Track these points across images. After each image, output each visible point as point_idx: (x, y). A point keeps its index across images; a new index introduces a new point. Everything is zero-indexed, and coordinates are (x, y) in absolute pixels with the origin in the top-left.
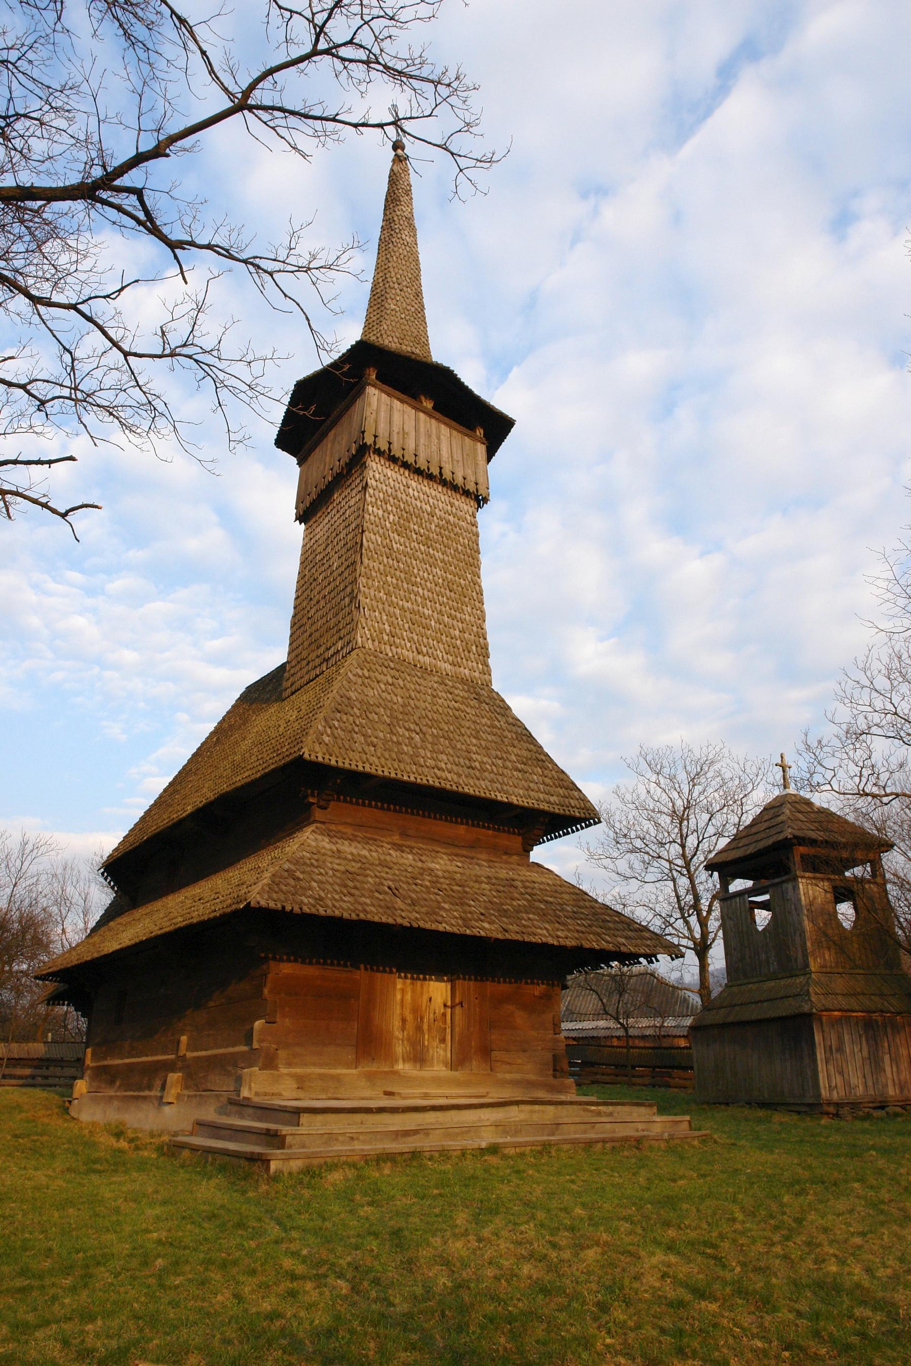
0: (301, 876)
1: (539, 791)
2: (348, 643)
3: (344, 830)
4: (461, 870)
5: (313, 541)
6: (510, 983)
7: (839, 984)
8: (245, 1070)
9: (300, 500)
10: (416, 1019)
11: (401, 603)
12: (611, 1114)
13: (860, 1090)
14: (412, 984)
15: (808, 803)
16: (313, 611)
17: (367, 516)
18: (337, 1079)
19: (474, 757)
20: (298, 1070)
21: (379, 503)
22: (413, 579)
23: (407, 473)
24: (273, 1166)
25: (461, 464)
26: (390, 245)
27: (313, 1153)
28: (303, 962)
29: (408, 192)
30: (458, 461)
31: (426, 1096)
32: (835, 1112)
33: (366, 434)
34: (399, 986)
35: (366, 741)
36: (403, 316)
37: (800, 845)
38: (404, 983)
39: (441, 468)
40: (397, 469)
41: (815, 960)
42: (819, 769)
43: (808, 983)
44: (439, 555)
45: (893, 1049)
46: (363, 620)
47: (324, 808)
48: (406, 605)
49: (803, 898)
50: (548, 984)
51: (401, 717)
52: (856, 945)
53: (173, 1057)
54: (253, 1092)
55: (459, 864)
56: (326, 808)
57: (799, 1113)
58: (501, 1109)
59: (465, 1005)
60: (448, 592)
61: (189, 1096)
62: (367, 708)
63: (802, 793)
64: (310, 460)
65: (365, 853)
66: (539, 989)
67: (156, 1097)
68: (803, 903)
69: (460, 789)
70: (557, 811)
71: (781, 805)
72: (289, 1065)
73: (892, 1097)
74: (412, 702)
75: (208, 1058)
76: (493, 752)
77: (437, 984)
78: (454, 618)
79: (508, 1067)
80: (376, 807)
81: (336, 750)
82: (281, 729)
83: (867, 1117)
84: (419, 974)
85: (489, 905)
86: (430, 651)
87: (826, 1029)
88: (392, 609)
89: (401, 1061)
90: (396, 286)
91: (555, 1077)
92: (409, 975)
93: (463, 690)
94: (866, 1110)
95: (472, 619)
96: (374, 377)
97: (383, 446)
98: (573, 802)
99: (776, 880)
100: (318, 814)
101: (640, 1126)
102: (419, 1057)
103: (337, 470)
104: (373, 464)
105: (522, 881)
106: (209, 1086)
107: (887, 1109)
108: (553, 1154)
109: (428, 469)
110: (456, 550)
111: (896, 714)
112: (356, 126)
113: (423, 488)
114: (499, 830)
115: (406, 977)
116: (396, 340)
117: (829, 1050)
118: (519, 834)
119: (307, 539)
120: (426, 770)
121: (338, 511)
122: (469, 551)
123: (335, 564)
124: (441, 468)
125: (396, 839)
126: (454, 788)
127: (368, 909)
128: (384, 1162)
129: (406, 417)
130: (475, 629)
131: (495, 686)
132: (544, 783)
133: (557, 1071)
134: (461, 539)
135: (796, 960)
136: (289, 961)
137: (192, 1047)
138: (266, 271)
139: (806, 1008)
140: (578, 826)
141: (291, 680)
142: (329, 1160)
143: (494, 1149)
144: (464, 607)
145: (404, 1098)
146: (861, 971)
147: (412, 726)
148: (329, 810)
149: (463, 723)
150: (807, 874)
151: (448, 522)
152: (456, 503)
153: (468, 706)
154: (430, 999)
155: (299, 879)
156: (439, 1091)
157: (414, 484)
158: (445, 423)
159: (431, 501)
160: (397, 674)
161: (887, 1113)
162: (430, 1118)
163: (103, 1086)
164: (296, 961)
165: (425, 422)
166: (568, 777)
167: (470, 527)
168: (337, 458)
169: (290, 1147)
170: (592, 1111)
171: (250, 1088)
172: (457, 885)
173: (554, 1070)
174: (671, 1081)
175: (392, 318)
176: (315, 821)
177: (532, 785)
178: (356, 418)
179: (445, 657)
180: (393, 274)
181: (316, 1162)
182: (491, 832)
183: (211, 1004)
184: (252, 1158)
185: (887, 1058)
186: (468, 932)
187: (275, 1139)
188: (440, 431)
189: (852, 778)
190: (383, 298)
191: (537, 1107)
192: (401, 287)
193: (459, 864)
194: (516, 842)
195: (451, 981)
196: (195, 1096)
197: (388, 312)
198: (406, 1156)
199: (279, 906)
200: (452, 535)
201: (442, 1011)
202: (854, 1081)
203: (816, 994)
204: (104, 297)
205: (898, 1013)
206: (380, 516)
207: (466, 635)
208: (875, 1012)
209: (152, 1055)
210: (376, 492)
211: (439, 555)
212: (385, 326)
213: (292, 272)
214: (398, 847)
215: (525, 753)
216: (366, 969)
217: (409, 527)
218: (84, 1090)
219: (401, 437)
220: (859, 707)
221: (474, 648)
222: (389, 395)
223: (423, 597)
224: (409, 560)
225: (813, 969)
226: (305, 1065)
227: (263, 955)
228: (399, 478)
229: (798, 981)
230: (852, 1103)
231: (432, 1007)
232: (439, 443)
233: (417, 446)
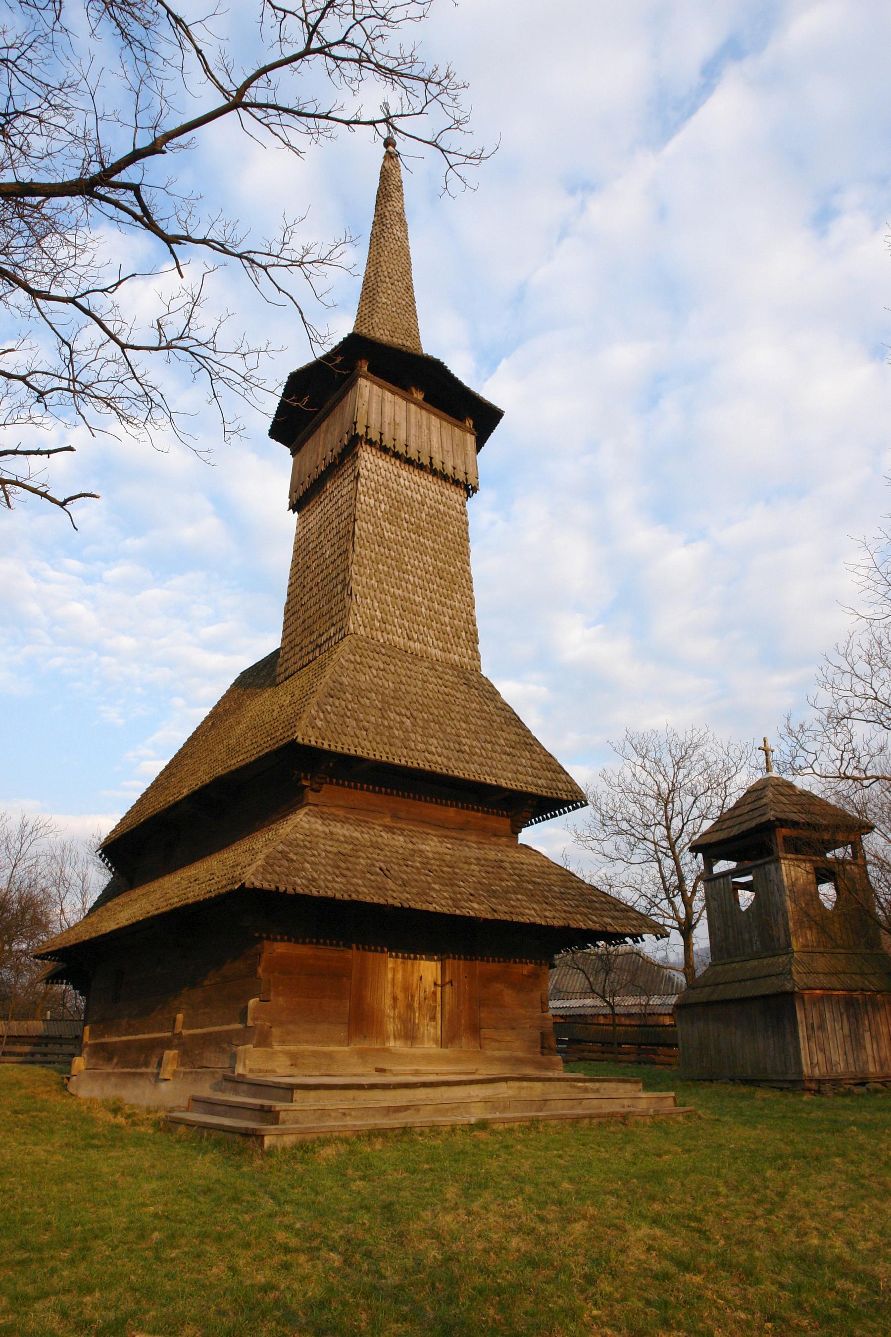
0: (295, 858)
1: (527, 774)
2: (340, 630)
3: (337, 813)
4: (451, 852)
5: (306, 529)
6: (499, 962)
7: (821, 963)
8: (240, 1048)
9: (293, 489)
11: (392, 590)
12: (598, 1091)
13: (842, 1067)
14: (403, 963)
15: (791, 786)
16: (306, 598)
17: (359, 505)
18: (330, 1056)
19: (464, 740)
20: (292, 1048)
21: (371, 492)
22: (404, 567)
23: (398, 463)
24: (268, 1141)
25: (451, 454)
26: (382, 240)
27: (306, 1128)
28: (296, 942)
29: (399, 188)
30: (448, 452)
31: (416, 1073)
32: (816, 1088)
34: (390, 965)
36: (394, 309)
37: (782, 827)
38: (396, 962)
39: (431, 458)
40: (388, 459)
41: (797, 939)
42: (801, 752)
43: (790, 963)
44: (429, 543)
46: (355, 607)
49: (785, 879)
50: (536, 964)
52: (837, 925)
53: (169, 1034)
54: (247, 1069)
55: (449, 846)
57: (781, 1089)
58: (490, 1086)
59: (455, 984)
60: (438, 579)
61: (185, 1073)
62: (359, 693)
63: (784, 776)
64: (303, 450)
65: (357, 834)
66: (527, 968)
67: (153, 1073)
68: (786, 883)
69: (450, 773)
70: (544, 794)
71: (764, 788)
72: (283, 1042)
73: (872, 1073)
74: (403, 687)
75: (203, 1036)
77: (428, 963)
78: (444, 605)
79: (497, 1044)
80: (368, 790)
83: (848, 1094)
86: (421, 637)
88: (383, 596)
89: (392, 1038)
90: (387, 280)
91: (543, 1054)
92: (400, 955)
93: (453, 675)
94: (847, 1086)
95: (462, 606)
96: (366, 369)
97: (375, 437)
98: (560, 785)
99: (759, 862)
100: (311, 797)
102: (410, 1035)
103: (329, 460)
104: (365, 454)
105: (511, 862)
106: (205, 1063)
108: (541, 1129)
109: (419, 459)
110: (446, 538)
111: (876, 698)
112: (348, 123)
113: (414, 477)
114: (488, 813)
115: (397, 957)
116: (388, 333)
117: (811, 1027)
118: (508, 817)
119: (300, 528)
120: (416, 754)
121: (331, 501)
122: (458, 539)
124: (431, 458)
125: (387, 821)
126: (444, 771)
127: (360, 889)
129: (397, 408)
130: (464, 615)
131: (484, 672)
132: (532, 767)
133: (545, 1049)
134: (451, 527)
135: (778, 940)
136: (282, 940)
137: (187, 1025)
138: (260, 266)
139: (788, 987)
141: (284, 666)
143: (483, 1125)
144: (454, 594)
145: (396, 1075)
146: (842, 951)
147: (403, 711)
148: (322, 793)
149: (453, 707)
150: (789, 856)
151: (438, 511)
152: (446, 492)
153: (458, 691)
154: (421, 978)
155: (292, 860)
156: (438, 1068)
157: (405, 474)
158: (435, 414)
159: (422, 490)
161: (868, 1090)
162: (421, 1094)
163: (101, 1063)
164: (289, 940)
165: (416, 413)
166: (556, 761)
167: (459, 516)
168: (329, 449)
169: (284, 1122)
170: (579, 1088)
171: (245, 1065)
172: (447, 866)
173: (542, 1047)
174: (657, 1058)
175: (384, 312)
176: (308, 804)
177: (520, 768)
178: (348, 409)
179: (436, 643)
181: (309, 1137)
182: (480, 814)
183: (207, 982)
184: (247, 1134)
185: (867, 1035)
186: (458, 912)
187: (269, 1115)
188: (430, 422)
189: (833, 761)
190: (375, 292)
191: (525, 1084)
192: (392, 281)
193: (449, 846)
194: (505, 824)
195: (441, 960)
196: (191, 1072)
197: (380, 305)
198: (397, 1131)
199: (273, 887)
200: (442, 524)
201: (433, 989)
202: (835, 1058)
203: (799, 973)
204: (102, 291)
205: (879, 992)
206: (372, 505)
207: (456, 622)
208: (855, 991)
209: (148, 1033)
210: (368, 482)
211: (429, 543)
212: (377, 319)
213: (286, 266)
214: (389, 829)
215: (513, 737)
216: (358, 948)
217: (400, 516)
218: (83, 1067)
219: (392, 427)
220: (840, 692)
221: (463, 634)
222: (380, 386)
223: (414, 584)
225: (795, 949)
226: (298, 1042)
227: (257, 935)
228: (391, 468)
230: (833, 1080)
231: (422, 986)
232: (430, 434)
233: (407, 436)
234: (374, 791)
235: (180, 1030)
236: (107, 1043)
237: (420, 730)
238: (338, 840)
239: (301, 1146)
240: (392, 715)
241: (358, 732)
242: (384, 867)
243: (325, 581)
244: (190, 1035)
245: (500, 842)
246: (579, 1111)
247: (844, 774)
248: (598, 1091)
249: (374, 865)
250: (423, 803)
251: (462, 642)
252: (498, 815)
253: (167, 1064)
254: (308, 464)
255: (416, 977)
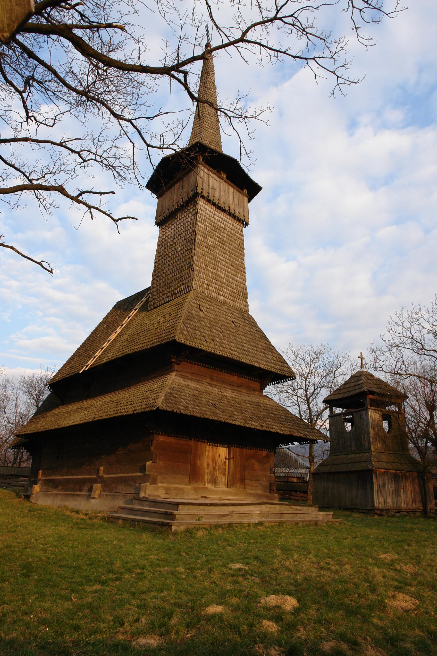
0: (176, 396)
1: (271, 363)
2: (188, 287)
3: (187, 375)
4: (237, 397)
6: (253, 449)
7: (384, 457)
8: (142, 484)
9: (158, 215)
10: (213, 464)
11: (211, 270)
12: (301, 510)
13: (390, 505)
14: (212, 448)
15: (372, 376)
16: (166, 269)
17: (197, 227)
18: (182, 490)
19: (245, 345)
20: (166, 485)
22: (217, 259)
23: (214, 208)
24: (174, 528)
25: (238, 206)
26: (205, 95)
27: (190, 523)
28: (168, 436)
29: (213, 70)
31: (220, 499)
32: (380, 513)
33: (198, 188)
34: (207, 449)
35: (201, 335)
36: (211, 131)
37: (370, 394)
38: (209, 448)
39: (229, 207)
41: (373, 446)
42: (378, 361)
43: (370, 456)
44: (227, 249)
45: (405, 488)
46: (195, 277)
47: (178, 364)
48: (214, 271)
49: (370, 418)
50: (268, 451)
51: (214, 324)
52: (391, 441)
53: (95, 476)
54: (147, 495)
55: (237, 394)
56: (179, 365)
57: (363, 513)
58: (259, 506)
60: (231, 266)
61: (106, 495)
62: (200, 319)
63: (369, 371)
64: (164, 196)
65: (198, 386)
66: (265, 453)
67: (85, 495)
68: (370, 420)
69: (240, 360)
70: (279, 372)
71: (360, 376)
72: (162, 483)
73: (403, 508)
74: (217, 317)
75: (117, 478)
76: (252, 343)
77: (223, 448)
78: (233, 279)
79: (251, 487)
80: (200, 365)
81: (189, 338)
82: (155, 325)
83: (393, 516)
84: (215, 443)
85: (252, 414)
86: (223, 294)
87: (378, 477)
88: (208, 273)
89: (207, 483)
90: (208, 116)
91: (270, 493)
92: (211, 444)
93: (237, 313)
94: (393, 513)
95: (241, 280)
97: (206, 194)
98: (285, 369)
99: (357, 410)
100: (176, 367)
101: (314, 516)
102: (214, 482)
103: (180, 202)
104: (200, 202)
105: (263, 404)
106: (118, 491)
107: (401, 513)
108: (285, 526)
110: (235, 247)
111: (412, 338)
112: (294, 57)
114: (250, 380)
115: (210, 445)
116: (209, 143)
117: (379, 486)
118: (259, 382)
119: (161, 235)
120: (226, 350)
123: (179, 249)
124: (229, 207)
125: (208, 380)
126: (238, 359)
127: (207, 413)
128: (219, 527)
130: (242, 285)
131: (250, 313)
132: (273, 360)
133: (271, 491)
135: (365, 446)
136: (162, 435)
137: (107, 471)
138: (228, 116)
139: (370, 467)
140: (285, 380)
141: (153, 302)
142: (195, 526)
143: (261, 524)
144: (237, 274)
145: (212, 500)
146: (392, 452)
147: (219, 329)
148: (180, 365)
149: (239, 329)
150: (372, 408)
151: (231, 233)
153: (240, 321)
154: (220, 455)
155: (175, 397)
156: (229, 497)
157: (217, 214)
158: (231, 186)
159: (224, 222)
160: (211, 304)
161: (401, 515)
162: (231, 509)
163: (51, 488)
164: (165, 435)
166: (282, 357)
167: (240, 236)
169: (177, 520)
170: (294, 508)
171: (145, 493)
172: (238, 404)
173: (270, 490)
174: (292, 497)
175: (207, 132)
176: (174, 370)
177: (268, 360)
178: (192, 179)
179: (230, 297)
180: (207, 110)
181: (191, 527)
182: (247, 380)
183: (118, 453)
184: (163, 525)
185: (402, 490)
186: (247, 426)
187: (172, 516)
188: (229, 190)
189: (391, 366)
191: (272, 506)
192: (210, 116)
193: (237, 394)
194: (257, 385)
195: (229, 448)
197: (205, 128)
198: (226, 525)
199: (171, 410)
200: (233, 240)
201: (224, 461)
202: (389, 500)
203: (374, 461)
204: (147, 118)
205: (409, 471)
207: (238, 288)
208: (398, 470)
209: (81, 475)
211: (227, 249)
213: (238, 118)
214: (210, 385)
215: (264, 345)
216: (194, 440)
218: (38, 490)
220: (396, 334)
221: (241, 294)
223: (221, 268)
224: (215, 250)
225: (373, 450)
226: (168, 483)
227: (151, 431)
228: (211, 210)
229: (365, 455)
230: (387, 510)
231: (220, 459)
232: (229, 195)
233: (219, 195)
234: (203, 366)
235: (102, 475)
236: (55, 479)
237: (226, 339)
238: (191, 389)
239: (187, 530)
240: (215, 331)
241: (201, 338)
242: (213, 403)
243: (177, 263)
244: (108, 477)
245: (255, 393)
246: (296, 519)
247: (397, 372)
248: (301, 510)
249: (209, 402)
250: (223, 373)
251: (241, 298)
252: (255, 381)
253: (96, 491)
254: (167, 204)
255: (218, 454)
